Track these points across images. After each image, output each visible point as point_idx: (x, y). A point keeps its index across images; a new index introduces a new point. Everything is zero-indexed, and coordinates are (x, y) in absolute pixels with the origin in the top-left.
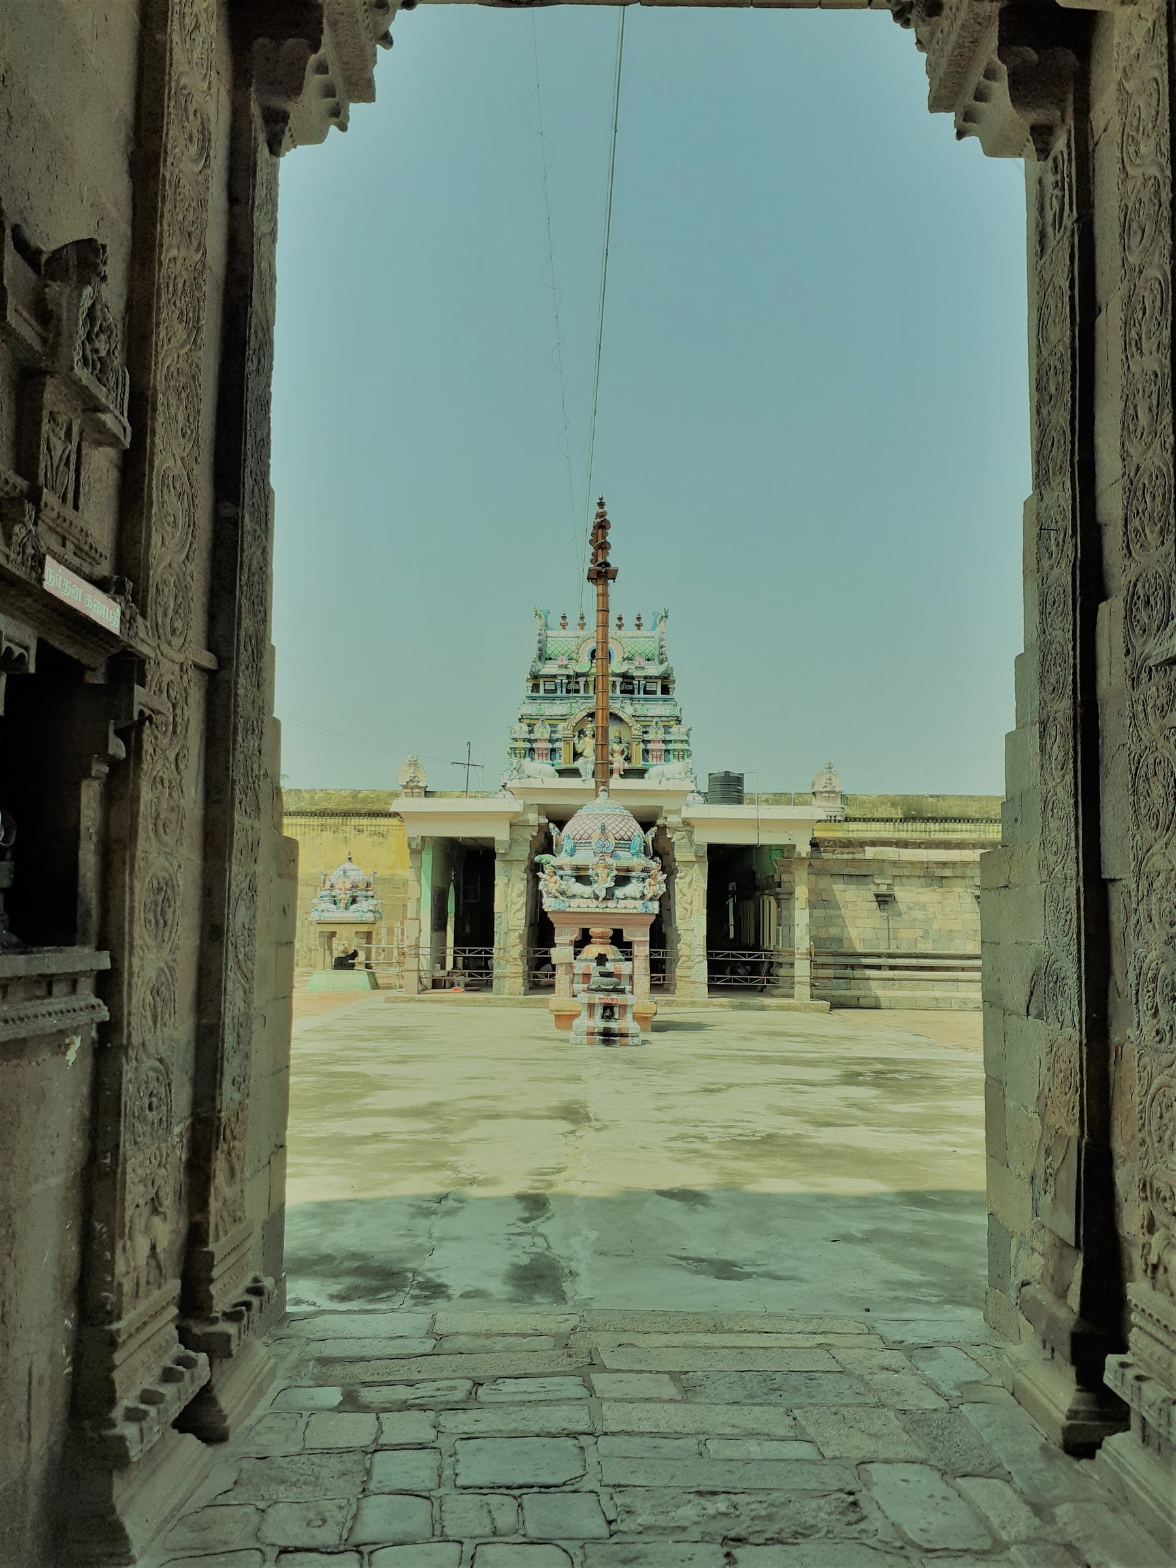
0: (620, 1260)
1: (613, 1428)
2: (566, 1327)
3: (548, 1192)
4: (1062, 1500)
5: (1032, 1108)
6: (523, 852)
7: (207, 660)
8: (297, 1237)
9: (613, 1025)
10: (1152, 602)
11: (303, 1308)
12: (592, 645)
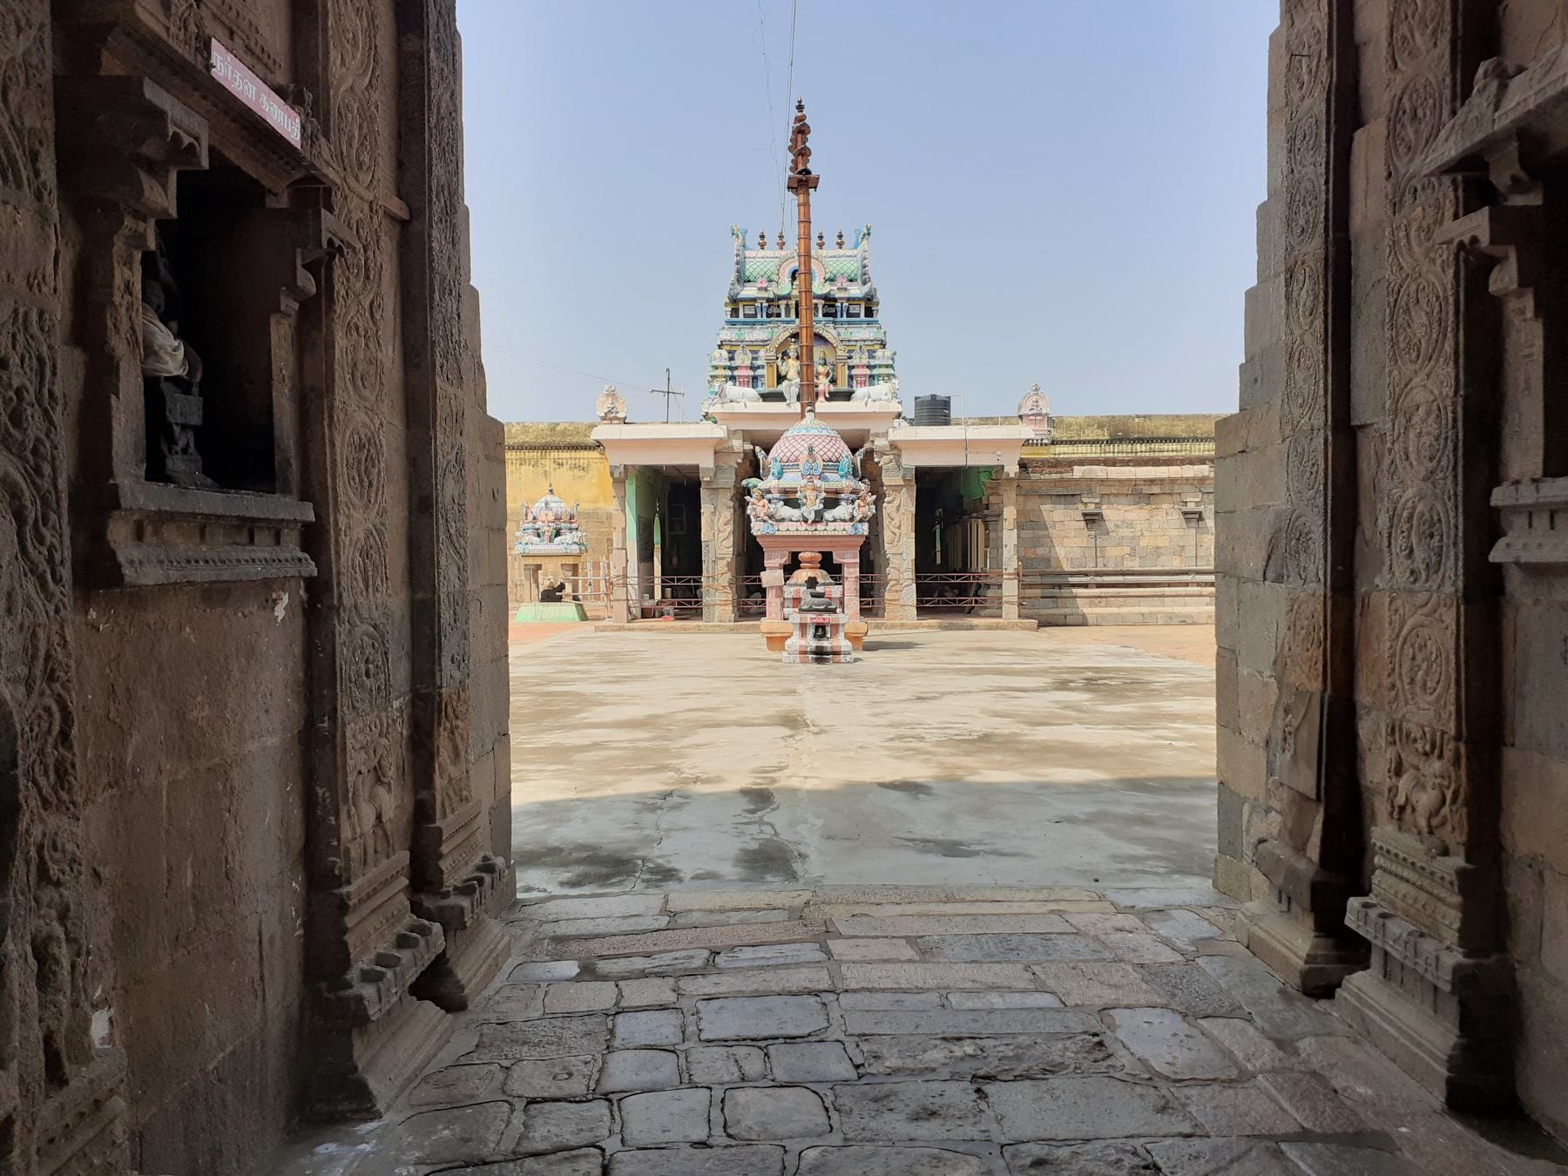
0: (847, 844)
1: (853, 986)
2: (799, 902)
3: (771, 787)
4: (1304, 1036)
5: (1267, 673)
6: (728, 480)
7: (398, 208)
8: (523, 834)
9: (825, 644)
10: (1420, 114)
11: (534, 895)
12: (795, 265)
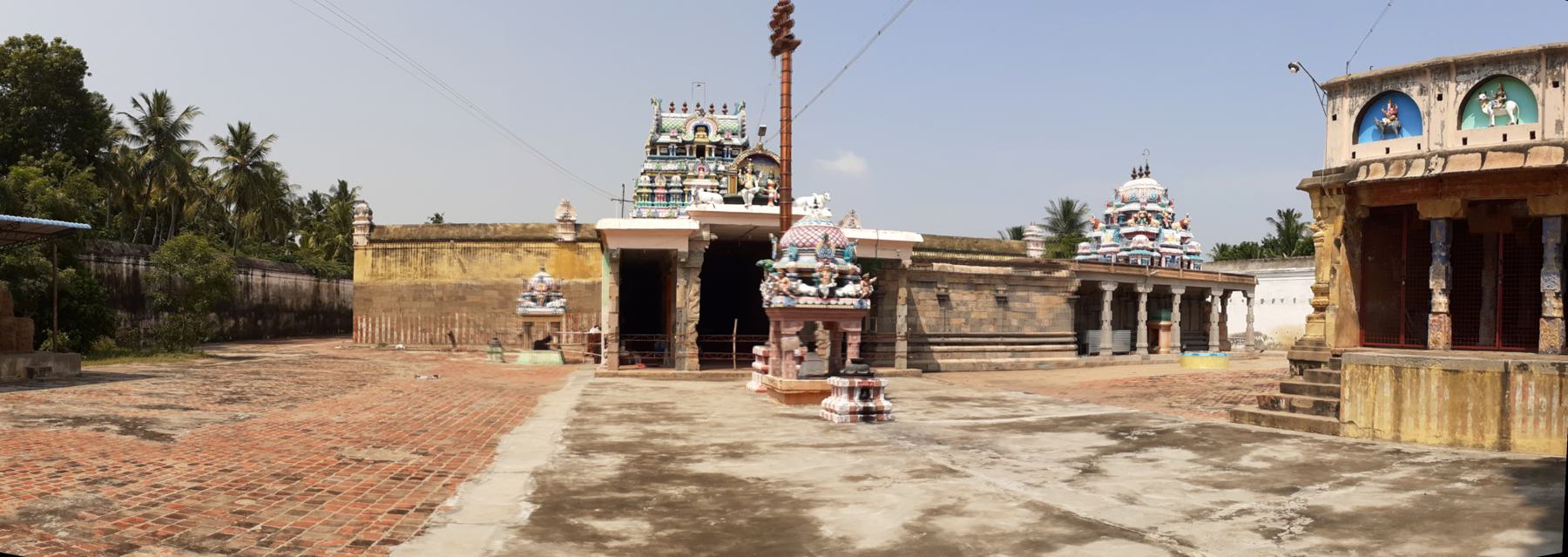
9: (871, 405)
